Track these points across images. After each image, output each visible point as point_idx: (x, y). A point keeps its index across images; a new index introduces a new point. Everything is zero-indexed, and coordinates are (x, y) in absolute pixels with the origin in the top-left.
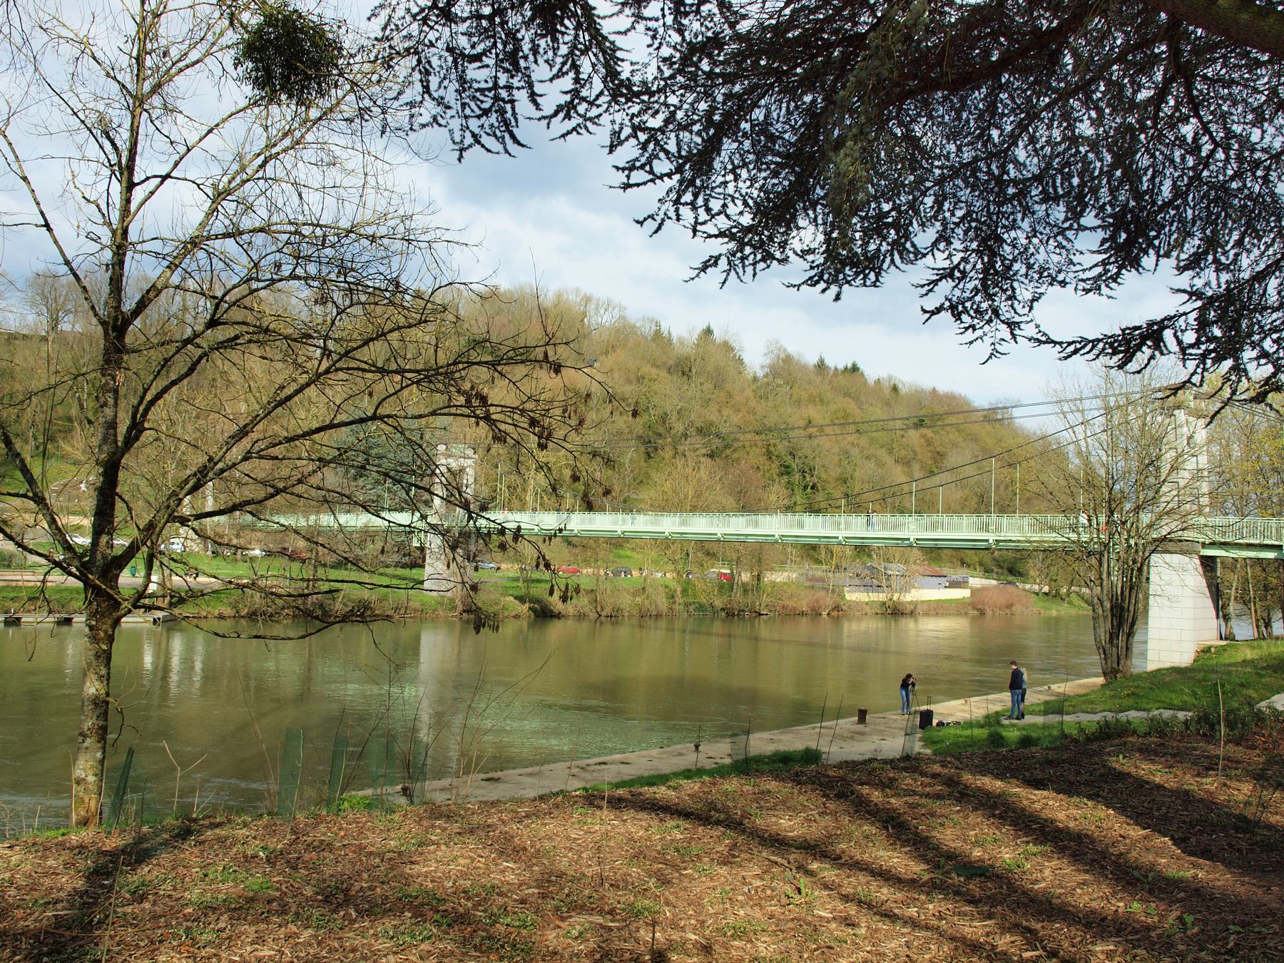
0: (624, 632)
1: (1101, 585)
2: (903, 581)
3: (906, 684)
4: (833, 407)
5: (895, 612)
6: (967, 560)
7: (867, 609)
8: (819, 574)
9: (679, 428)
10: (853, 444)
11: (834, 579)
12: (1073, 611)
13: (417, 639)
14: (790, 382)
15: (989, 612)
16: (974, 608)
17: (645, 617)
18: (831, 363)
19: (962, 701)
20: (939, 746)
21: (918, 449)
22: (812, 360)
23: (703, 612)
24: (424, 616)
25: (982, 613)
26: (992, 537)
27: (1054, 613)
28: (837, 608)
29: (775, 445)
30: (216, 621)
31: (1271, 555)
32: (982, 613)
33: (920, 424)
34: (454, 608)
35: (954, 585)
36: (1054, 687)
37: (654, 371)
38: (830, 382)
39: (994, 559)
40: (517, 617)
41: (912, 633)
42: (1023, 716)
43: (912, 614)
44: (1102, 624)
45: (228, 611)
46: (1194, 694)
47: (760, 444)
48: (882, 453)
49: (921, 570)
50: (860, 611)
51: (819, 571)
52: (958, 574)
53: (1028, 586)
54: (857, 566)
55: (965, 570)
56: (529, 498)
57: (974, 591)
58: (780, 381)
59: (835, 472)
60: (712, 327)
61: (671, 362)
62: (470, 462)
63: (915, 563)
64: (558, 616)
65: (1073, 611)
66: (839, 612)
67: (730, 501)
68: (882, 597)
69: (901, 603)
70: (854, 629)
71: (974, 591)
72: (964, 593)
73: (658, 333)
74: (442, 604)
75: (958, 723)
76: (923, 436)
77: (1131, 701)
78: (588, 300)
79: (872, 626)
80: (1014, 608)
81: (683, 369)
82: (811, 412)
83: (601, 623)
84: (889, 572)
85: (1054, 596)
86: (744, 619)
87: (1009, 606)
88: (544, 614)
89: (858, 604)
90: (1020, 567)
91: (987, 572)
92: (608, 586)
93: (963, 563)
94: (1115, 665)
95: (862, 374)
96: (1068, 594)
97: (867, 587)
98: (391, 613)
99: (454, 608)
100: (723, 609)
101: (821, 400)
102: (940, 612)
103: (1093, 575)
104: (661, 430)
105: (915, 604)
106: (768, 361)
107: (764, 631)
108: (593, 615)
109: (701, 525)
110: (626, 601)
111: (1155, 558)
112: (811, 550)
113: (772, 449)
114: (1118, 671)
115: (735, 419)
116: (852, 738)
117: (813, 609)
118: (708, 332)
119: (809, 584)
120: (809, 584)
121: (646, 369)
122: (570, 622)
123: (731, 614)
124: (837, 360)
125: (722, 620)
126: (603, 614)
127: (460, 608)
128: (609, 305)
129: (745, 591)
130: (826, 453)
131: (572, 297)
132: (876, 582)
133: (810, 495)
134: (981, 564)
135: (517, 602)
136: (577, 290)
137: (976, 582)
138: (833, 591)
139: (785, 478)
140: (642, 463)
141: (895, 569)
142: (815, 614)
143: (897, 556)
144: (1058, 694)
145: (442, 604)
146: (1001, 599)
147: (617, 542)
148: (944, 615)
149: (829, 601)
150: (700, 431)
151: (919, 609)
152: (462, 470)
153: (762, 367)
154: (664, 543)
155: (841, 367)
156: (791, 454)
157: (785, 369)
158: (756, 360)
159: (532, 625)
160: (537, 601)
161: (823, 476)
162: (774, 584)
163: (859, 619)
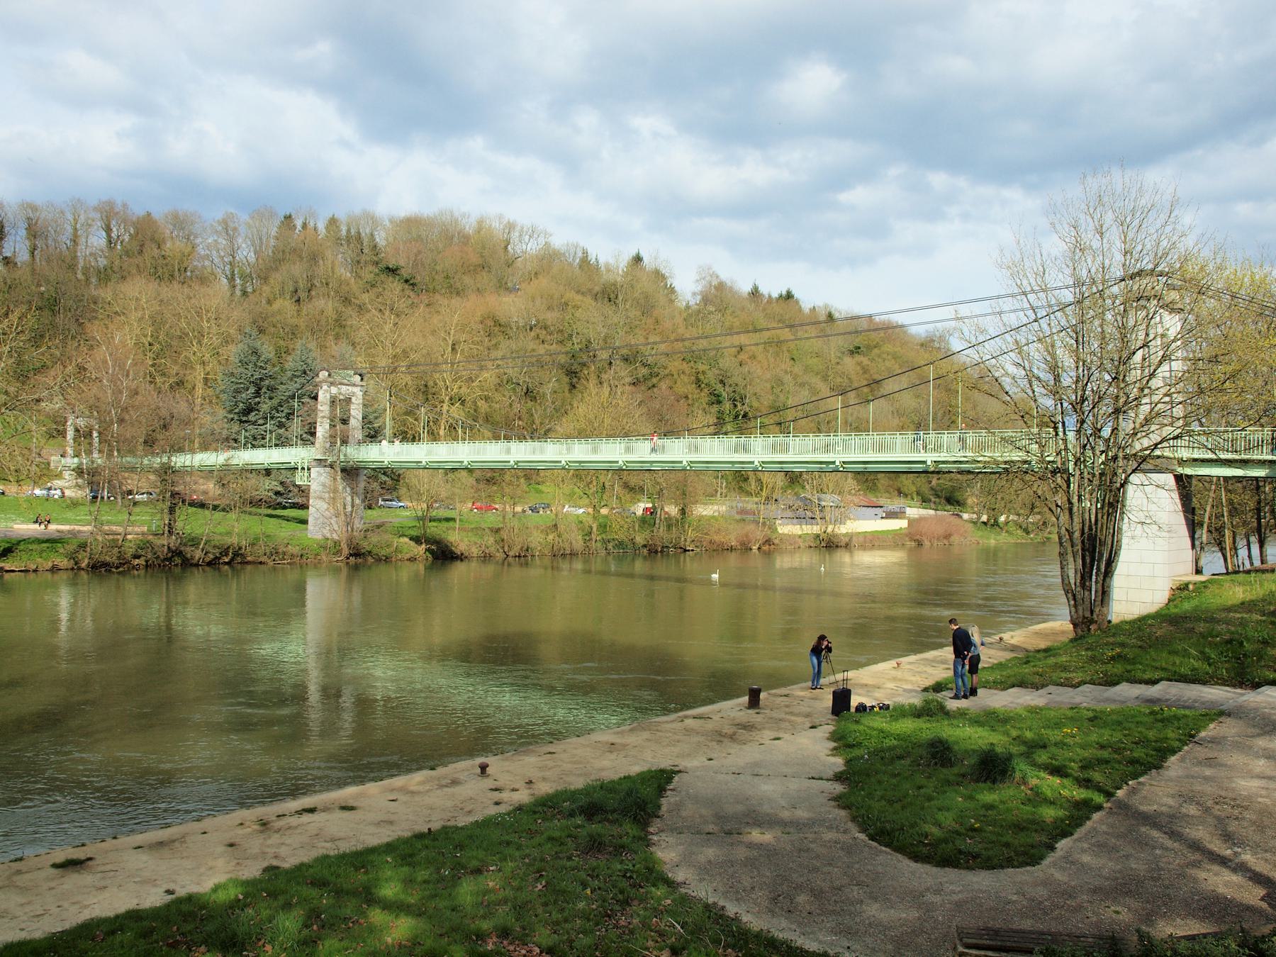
0: (535, 572)
1: (1071, 510)
3: (820, 650)
5: (829, 545)
6: (905, 490)
8: (750, 506)
10: (786, 372)
11: (767, 511)
12: (1011, 540)
13: (301, 589)
14: (722, 309)
15: (927, 543)
17: (560, 555)
18: (764, 290)
19: (893, 663)
20: (857, 752)
21: (853, 377)
22: (746, 288)
23: (624, 550)
24: (303, 561)
25: (920, 544)
26: (930, 458)
28: (768, 541)
29: (704, 373)
30: (49, 575)
31: (1260, 473)
32: (920, 544)
33: (856, 351)
34: (339, 552)
35: (891, 515)
36: (1006, 636)
37: (579, 297)
38: (764, 310)
39: (932, 489)
40: (412, 560)
41: (847, 570)
42: (973, 692)
44: (1071, 559)
45: (64, 563)
46: (1207, 659)
48: (817, 382)
49: (856, 500)
50: (793, 544)
51: (750, 503)
52: (895, 504)
54: (789, 498)
55: (902, 500)
56: (442, 432)
57: (911, 522)
58: (712, 309)
59: (767, 400)
60: (642, 254)
61: (597, 289)
62: (357, 390)
63: (850, 493)
64: (461, 558)
66: (770, 546)
67: (650, 428)
68: (816, 529)
69: (835, 535)
70: (783, 562)
71: (911, 522)
72: (903, 524)
73: (585, 261)
74: (325, 548)
75: (885, 707)
76: (859, 364)
77: (1118, 669)
78: (511, 226)
79: (804, 559)
80: (952, 539)
81: (609, 295)
83: (509, 565)
84: (823, 503)
86: (668, 555)
87: (948, 536)
88: (443, 555)
89: (791, 538)
90: (958, 496)
91: (925, 501)
92: (516, 523)
94: (1088, 614)
95: (797, 302)
97: (800, 519)
98: (263, 559)
99: (339, 552)
100: (645, 546)
102: (876, 543)
103: (1060, 499)
104: (585, 359)
105: (851, 536)
106: (700, 288)
107: (690, 565)
108: (500, 556)
109: (613, 452)
110: (537, 540)
111: (1135, 478)
112: (740, 479)
113: (701, 377)
114: (1092, 621)
116: (732, 737)
117: (743, 544)
118: (638, 259)
119: (738, 517)
120: (738, 517)
121: (571, 295)
122: (474, 564)
123: (653, 551)
124: (772, 288)
125: (645, 558)
126: (511, 553)
127: (346, 551)
129: (669, 527)
130: (759, 377)
131: (496, 224)
132: (809, 514)
133: (734, 415)
135: (412, 543)
136: (500, 217)
137: (914, 512)
138: (764, 524)
139: (715, 408)
140: (567, 394)
141: (829, 500)
143: (831, 485)
145: (325, 548)
147: (530, 474)
148: (881, 548)
149: (759, 535)
150: (626, 360)
152: (348, 400)
153: (694, 294)
154: (581, 474)
155: (775, 295)
156: (722, 382)
157: (717, 297)
158: (687, 287)
159: (429, 568)
160: (437, 542)
161: (755, 404)
162: (701, 518)
163: (792, 553)
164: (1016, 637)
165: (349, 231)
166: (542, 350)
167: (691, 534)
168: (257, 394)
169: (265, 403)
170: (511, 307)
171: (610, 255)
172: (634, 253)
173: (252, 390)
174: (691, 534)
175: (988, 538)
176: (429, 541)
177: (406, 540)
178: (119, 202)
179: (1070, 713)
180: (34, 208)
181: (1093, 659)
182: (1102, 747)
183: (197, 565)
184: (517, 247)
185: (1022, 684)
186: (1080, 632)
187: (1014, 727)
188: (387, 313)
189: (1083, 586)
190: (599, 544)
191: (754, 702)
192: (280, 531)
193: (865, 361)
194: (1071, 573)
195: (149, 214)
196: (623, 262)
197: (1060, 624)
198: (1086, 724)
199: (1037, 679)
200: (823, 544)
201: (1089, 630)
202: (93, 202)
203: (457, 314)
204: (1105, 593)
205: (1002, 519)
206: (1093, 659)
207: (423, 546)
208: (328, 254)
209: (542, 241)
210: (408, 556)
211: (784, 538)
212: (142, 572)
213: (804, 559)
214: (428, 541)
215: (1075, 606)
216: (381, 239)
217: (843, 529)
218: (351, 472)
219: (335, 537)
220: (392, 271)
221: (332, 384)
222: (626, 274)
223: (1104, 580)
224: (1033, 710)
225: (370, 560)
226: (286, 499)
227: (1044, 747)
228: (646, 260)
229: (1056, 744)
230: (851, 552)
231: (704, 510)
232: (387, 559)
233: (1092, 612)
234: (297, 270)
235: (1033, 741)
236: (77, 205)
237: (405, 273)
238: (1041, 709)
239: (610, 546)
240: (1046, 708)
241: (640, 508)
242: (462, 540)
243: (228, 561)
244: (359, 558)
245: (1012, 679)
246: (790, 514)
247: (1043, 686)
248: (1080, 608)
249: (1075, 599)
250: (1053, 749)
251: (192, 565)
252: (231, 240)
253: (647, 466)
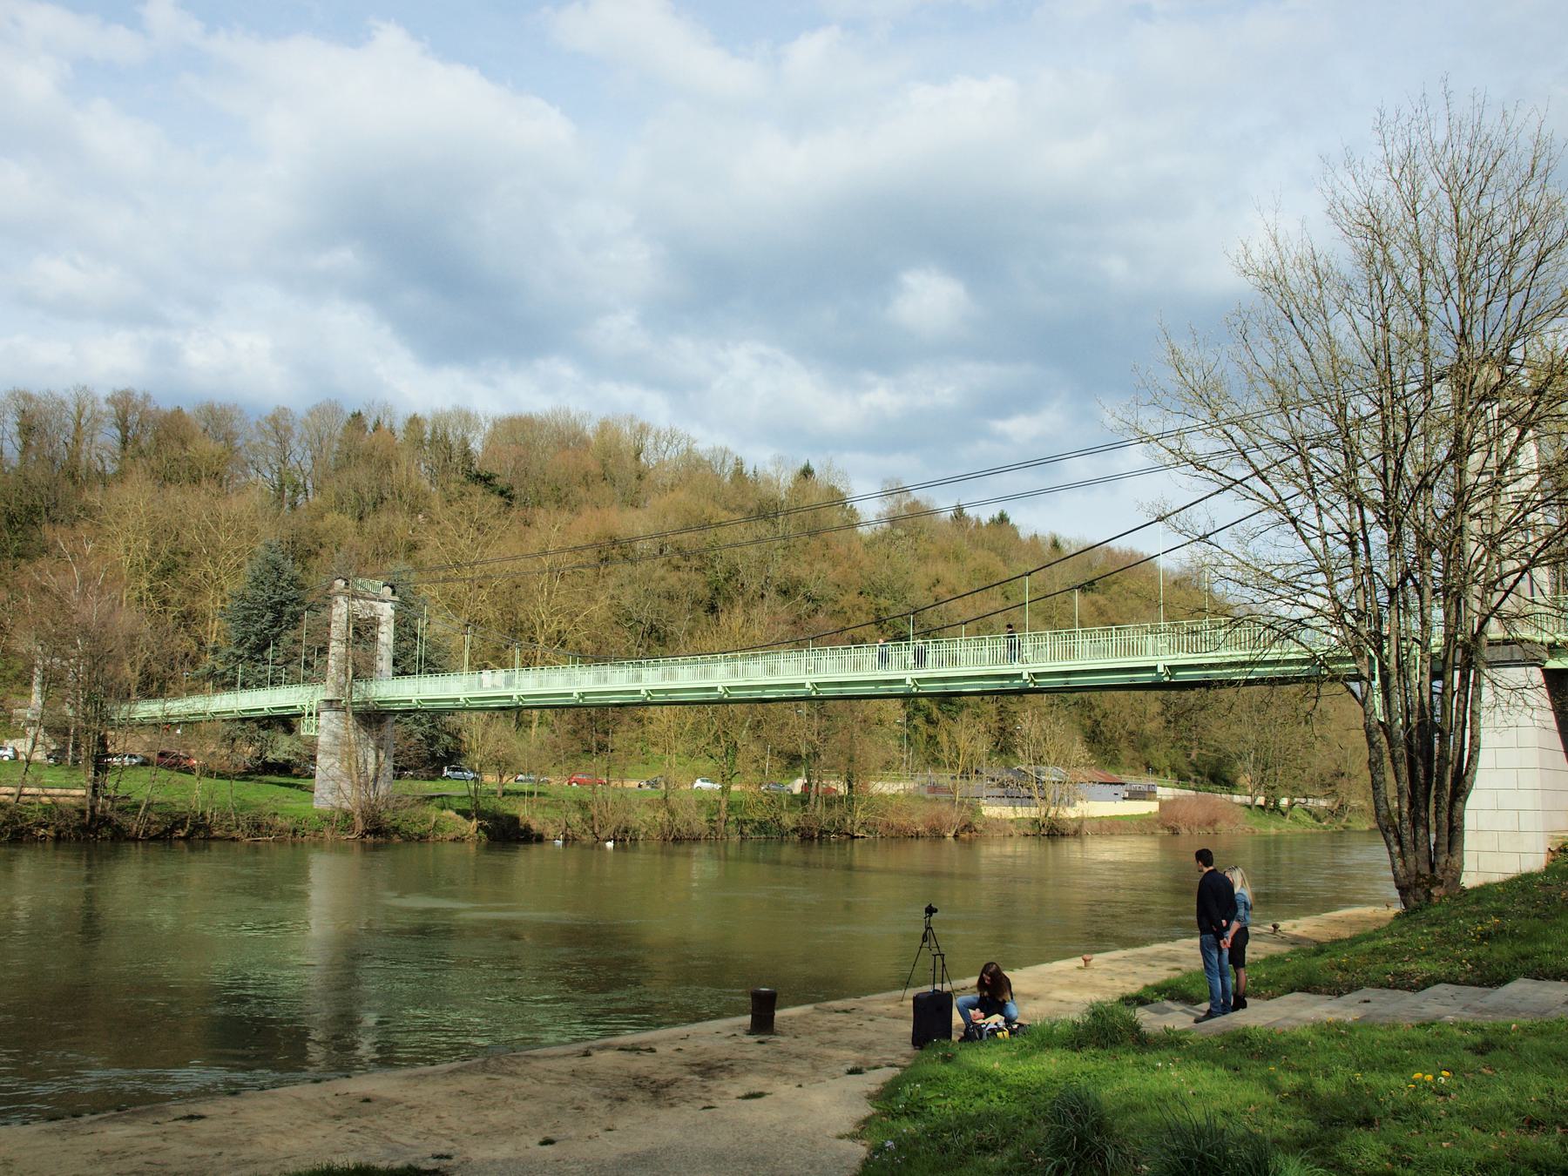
2: (1059, 790)
4: (970, 564)
5: (1053, 832)
6: (1155, 764)
7: (1012, 827)
9: (754, 586)
12: (1298, 829)
15: (1184, 831)
16: (1164, 827)
17: (677, 840)
19: (1079, 962)
24: (298, 837)
27: (1273, 831)
28: (968, 827)
32: (1175, 832)
34: (350, 828)
35: (1135, 795)
36: (1285, 925)
38: (970, 536)
39: (1191, 764)
40: (458, 840)
43: (1077, 834)
47: (865, 608)
51: (944, 778)
52: (1143, 781)
53: (1237, 799)
57: (1163, 804)
58: (899, 532)
60: (814, 465)
61: (751, 505)
65: (1298, 829)
66: (969, 833)
70: (992, 853)
73: (739, 473)
74: (330, 821)
76: (1094, 604)
78: (643, 430)
79: (1018, 850)
80: (1218, 826)
81: (767, 511)
82: (940, 568)
85: (1272, 809)
87: (1212, 823)
89: (999, 823)
91: (1182, 779)
93: (1148, 766)
96: (1291, 806)
97: (1012, 799)
99: (350, 828)
100: (795, 830)
101: (957, 557)
105: (1081, 821)
108: (588, 839)
115: (833, 576)
117: (932, 829)
118: (807, 472)
123: (808, 837)
127: (360, 826)
128: (672, 438)
133: (893, 625)
134: (1173, 770)
135: (460, 818)
137: (1166, 792)
141: (1051, 774)
142: (936, 835)
144: (1296, 941)
146: (1200, 814)
149: (955, 817)
150: (784, 592)
151: (1086, 828)
164: (1301, 926)
165: (434, 432)
166: (673, 579)
167: (860, 816)
168: (276, 621)
169: (275, 630)
170: (634, 523)
171: (770, 463)
172: (801, 466)
173: (269, 616)
174: (860, 816)
175: (1267, 826)
176: (481, 815)
177: (451, 813)
178: (139, 394)
179: (1420, 1035)
180: (28, 397)
181: (1447, 939)
182: (1532, 1124)
183: (135, 839)
184: (649, 458)
185: (1308, 986)
186: (1413, 903)
187: (1289, 1068)
188: (465, 525)
189: (1415, 821)
190: (731, 827)
191: (763, 1023)
192: (265, 795)
193: (1101, 600)
194: (1390, 788)
195: (179, 410)
196: (786, 479)
197: (1378, 906)
198: (1469, 1060)
199: (1338, 976)
200: (1044, 831)
201: (1429, 896)
202: (103, 393)
203: (553, 530)
204: (1454, 832)
205: (1284, 802)
206: (1447, 939)
207: (474, 822)
208: (403, 457)
209: (683, 446)
210: (452, 835)
211: (991, 823)
212: (50, 845)
213: (1018, 850)
214: (481, 815)
215: (1402, 854)
216: (476, 446)
217: (1071, 813)
218: (372, 718)
219: (346, 805)
220: (486, 480)
221: (354, 597)
222: (790, 492)
223: (1452, 805)
224: (1334, 1031)
225: (396, 839)
226: (274, 755)
227: (1367, 1122)
228: (817, 473)
229: (1396, 1114)
230: (1082, 843)
231: (884, 787)
232: (422, 838)
233: (1432, 867)
234: (362, 476)
235: (1335, 1103)
236: (83, 398)
237: (501, 483)
238: (1350, 1029)
239: (747, 830)
240: (1365, 1023)
241: (797, 786)
242: (533, 817)
243: (183, 833)
244: (378, 833)
245: (1291, 979)
246: (999, 791)
247: (1351, 988)
248: (1411, 858)
249: (1400, 843)
250: (1393, 1129)
251: (127, 839)
252: (282, 442)
253: (756, 694)
